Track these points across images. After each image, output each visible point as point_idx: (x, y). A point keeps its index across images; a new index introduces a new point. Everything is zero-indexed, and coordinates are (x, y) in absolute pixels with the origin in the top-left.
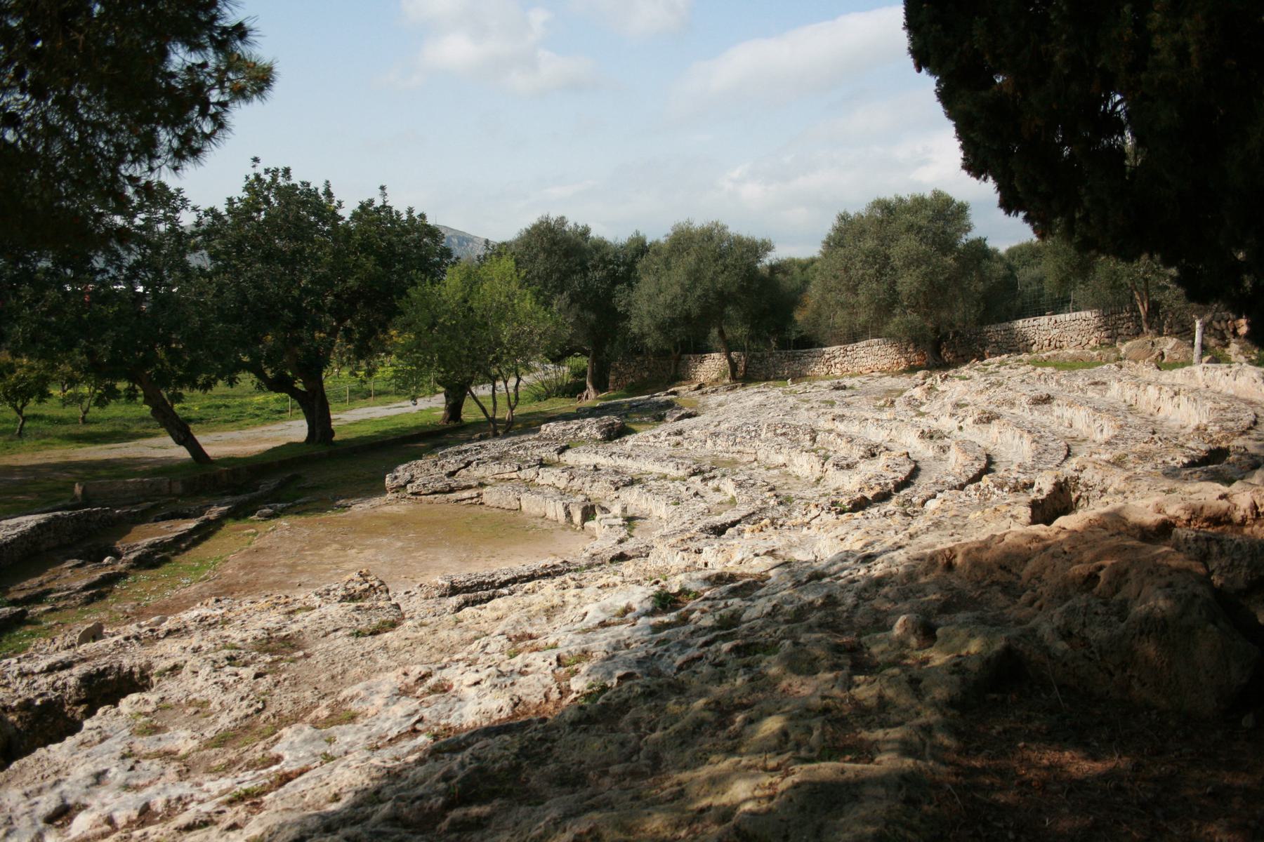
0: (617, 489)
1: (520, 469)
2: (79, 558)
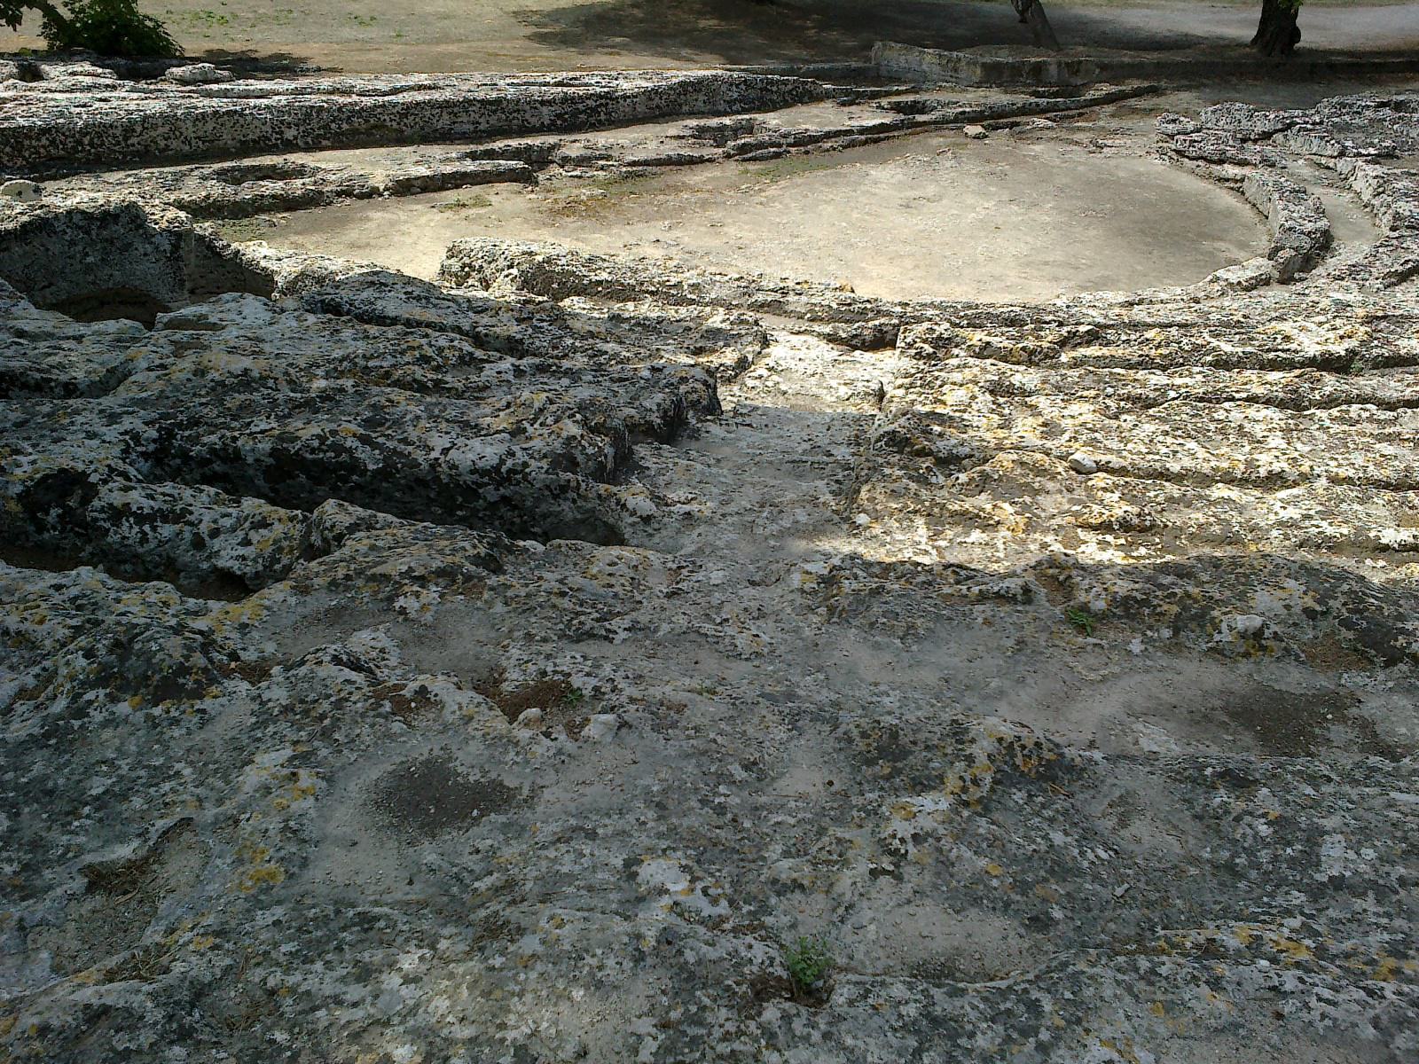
1: (1342, 154)
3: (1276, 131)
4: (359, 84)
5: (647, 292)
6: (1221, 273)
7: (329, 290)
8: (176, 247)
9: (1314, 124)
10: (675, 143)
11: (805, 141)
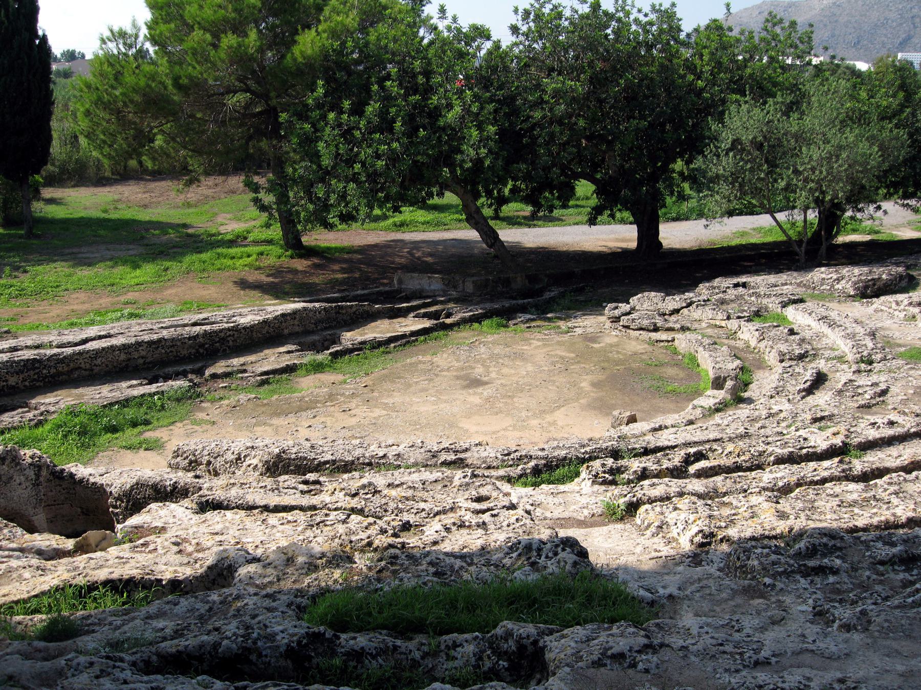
1: (729, 318)
2: (299, 344)
3: (683, 308)
4: (54, 338)
5: (364, 464)
6: (695, 402)
7: (207, 493)
8: (38, 476)
9: (704, 301)
10: (288, 356)
11: (377, 345)
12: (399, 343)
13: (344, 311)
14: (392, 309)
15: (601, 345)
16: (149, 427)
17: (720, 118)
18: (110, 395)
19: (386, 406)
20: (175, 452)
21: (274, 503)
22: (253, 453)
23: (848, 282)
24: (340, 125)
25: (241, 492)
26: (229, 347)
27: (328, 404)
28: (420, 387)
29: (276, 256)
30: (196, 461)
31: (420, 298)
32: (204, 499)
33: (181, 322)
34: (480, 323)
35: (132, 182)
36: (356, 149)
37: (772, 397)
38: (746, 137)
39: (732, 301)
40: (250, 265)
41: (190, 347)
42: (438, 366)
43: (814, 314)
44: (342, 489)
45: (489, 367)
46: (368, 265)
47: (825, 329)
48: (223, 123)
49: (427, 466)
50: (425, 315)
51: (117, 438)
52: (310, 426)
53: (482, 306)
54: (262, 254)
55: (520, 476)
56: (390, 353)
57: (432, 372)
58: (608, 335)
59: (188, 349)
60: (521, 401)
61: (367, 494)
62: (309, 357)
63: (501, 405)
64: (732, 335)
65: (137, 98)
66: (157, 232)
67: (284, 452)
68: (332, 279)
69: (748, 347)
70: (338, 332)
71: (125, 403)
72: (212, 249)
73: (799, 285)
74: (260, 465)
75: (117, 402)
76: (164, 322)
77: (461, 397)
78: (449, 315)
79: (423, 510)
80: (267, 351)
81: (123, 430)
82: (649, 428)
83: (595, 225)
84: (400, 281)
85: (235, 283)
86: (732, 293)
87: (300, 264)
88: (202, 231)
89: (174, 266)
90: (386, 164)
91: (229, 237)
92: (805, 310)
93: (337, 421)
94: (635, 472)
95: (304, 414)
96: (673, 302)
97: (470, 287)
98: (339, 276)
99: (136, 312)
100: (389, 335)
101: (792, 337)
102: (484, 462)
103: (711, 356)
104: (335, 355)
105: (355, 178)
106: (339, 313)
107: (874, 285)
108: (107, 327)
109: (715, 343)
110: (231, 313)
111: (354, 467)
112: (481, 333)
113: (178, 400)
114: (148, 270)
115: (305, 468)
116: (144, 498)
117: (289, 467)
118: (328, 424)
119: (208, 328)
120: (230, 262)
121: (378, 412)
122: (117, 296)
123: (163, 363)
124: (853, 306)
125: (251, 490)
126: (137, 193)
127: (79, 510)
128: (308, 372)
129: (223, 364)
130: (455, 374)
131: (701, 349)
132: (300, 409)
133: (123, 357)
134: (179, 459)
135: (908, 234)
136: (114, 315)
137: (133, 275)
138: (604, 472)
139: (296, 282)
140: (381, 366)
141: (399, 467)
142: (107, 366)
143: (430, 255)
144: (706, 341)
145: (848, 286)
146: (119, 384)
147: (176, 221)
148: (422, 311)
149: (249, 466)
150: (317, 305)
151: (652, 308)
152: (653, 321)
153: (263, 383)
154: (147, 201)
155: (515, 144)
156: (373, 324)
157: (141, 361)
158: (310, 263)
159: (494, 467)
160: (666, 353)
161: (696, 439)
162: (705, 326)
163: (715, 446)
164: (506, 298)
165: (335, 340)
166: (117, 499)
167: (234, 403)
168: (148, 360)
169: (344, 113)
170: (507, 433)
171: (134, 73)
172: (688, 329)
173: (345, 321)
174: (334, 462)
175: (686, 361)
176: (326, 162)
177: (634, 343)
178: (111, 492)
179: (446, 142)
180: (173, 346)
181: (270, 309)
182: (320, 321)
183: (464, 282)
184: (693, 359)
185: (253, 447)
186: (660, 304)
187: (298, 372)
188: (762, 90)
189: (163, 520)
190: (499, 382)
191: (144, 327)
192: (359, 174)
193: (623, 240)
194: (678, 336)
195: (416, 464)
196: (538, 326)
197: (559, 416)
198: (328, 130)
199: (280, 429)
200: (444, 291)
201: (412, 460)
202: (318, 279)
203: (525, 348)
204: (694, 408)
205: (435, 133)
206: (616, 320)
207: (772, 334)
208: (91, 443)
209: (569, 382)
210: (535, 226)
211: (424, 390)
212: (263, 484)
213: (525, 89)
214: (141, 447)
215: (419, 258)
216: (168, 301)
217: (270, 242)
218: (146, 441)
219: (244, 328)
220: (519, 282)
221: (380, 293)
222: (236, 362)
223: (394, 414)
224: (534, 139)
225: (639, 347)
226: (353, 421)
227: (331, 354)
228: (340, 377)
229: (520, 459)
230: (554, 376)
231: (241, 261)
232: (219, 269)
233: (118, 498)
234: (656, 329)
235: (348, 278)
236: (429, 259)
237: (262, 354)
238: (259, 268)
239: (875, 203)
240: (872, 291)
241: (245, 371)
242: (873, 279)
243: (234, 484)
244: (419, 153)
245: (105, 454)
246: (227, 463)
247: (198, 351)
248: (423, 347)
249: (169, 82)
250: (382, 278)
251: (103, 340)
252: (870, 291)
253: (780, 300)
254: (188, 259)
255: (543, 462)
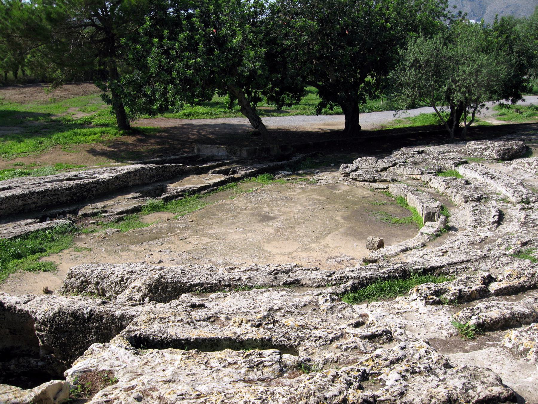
0: (466, 202)
1: (422, 174)
2: (140, 192)
5: (225, 286)
9: (403, 162)
10: (134, 201)
11: (192, 192)
12: (206, 191)
13: (168, 170)
14: (198, 168)
15: (340, 191)
16: (44, 254)
17: (404, 46)
18: (13, 231)
19: (210, 236)
20: (69, 274)
21: (194, 337)
22: (133, 276)
23: (492, 151)
24: (162, 46)
25: (162, 326)
26: (93, 195)
27: (169, 234)
28: (229, 221)
29: (113, 134)
30: (86, 281)
31: (213, 161)
32: (133, 335)
33: (58, 178)
34: (256, 177)
35: (11, 88)
36: (172, 63)
37: (475, 227)
38: (422, 59)
39: (421, 162)
40: (96, 140)
41: (67, 195)
42: (238, 207)
43: (478, 171)
44: (248, 321)
45: (272, 207)
46: (173, 140)
47: (488, 181)
48: (80, 45)
49: (272, 286)
50: (219, 172)
51: (22, 263)
52: (160, 251)
53: (255, 166)
54: (103, 132)
55: (344, 293)
56: (201, 197)
57: (235, 211)
58: (343, 185)
59: (65, 197)
60: (300, 230)
61: (268, 324)
62: (149, 202)
63: (288, 233)
64: (426, 184)
65: (22, 26)
66: (31, 119)
67: (162, 277)
68: (151, 149)
69: (438, 192)
70: (164, 183)
71: (26, 236)
72: (70, 129)
73: (459, 152)
74: (143, 287)
75: (19, 236)
76: (47, 178)
77: (259, 228)
78: (234, 172)
79: (320, 338)
80: (119, 198)
81: (26, 257)
82: (400, 249)
83: (320, 114)
84: (199, 150)
85: (88, 151)
86: (418, 158)
87: (130, 139)
88: (62, 118)
89: (47, 141)
90: (193, 73)
91: (79, 122)
92: (472, 168)
93: (178, 247)
94: (455, 293)
95: (154, 242)
96: (382, 163)
97: (244, 154)
98: (156, 147)
99: (25, 171)
100: (200, 186)
101: (469, 186)
102: (315, 282)
103: (418, 199)
104: (166, 200)
105: (172, 81)
106: (164, 171)
107: (509, 152)
108: (8, 181)
109: (417, 190)
110: (92, 171)
111: (217, 288)
112: (258, 184)
113: (63, 233)
114: (28, 144)
115: (179, 289)
116: (65, 323)
117: (167, 288)
118: (173, 249)
119: (79, 182)
120: (83, 138)
121: (205, 240)
122: (10, 160)
123: (49, 207)
124: (499, 166)
125: (170, 324)
126: (15, 94)
127: (8, 330)
128: (149, 212)
129: (90, 207)
130: (250, 212)
131: (409, 194)
132: (151, 239)
133: (21, 203)
134: (73, 279)
135: (495, 122)
136: (9, 174)
137: (19, 146)
138: (431, 294)
139: (128, 151)
140: (199, 207)
141: (251, 287)
142: (9, 209)
143: (211, 133)
144: (412, 189)
145: (493, 153)
146: (19, 222)
147: (43, 112)
148: (217, 169)
149: (134, 288)
150: (150, 166)
151: (368, 167)
152: (372, 175)
153: (120, 220)
154: (22, 100)
155: (273, 61)
156: (187, 178)
157: (33, 206)
158: (135, 138)
159: (322, 286)
160: (383, 197)
161: (455, 261)
162: (408, 177)
163: (469, 266)
164: (268, 160)
165: (164, 190)
166: (41, 324)
167: (103, 235)
168: (38, 205)
169: (165, 38)
170: (298, 254)
171: (20, 9)
172: (396, 181)
173: (169, 176)
174: (202, 284)
175: (399, 202)
176: (153, 70)
177: (361, 190)
178: (36, 318)
179: (231, 59)
180: (55, 195)
181: (119, 168)
182: (153, 177)
183: (240, 151)
184: (403, 201)
185: (132, 272)
186: (374, 164)
187: (143, 212)
188: (429, 30)
189: (108, 363)
190: (282, 217)
191: (33, 182)
192: (175, 79)
193: (328, 125)
194: (391, 185)
195: (264, 285)
196: (295, 179)
197: (329, 240)
198: (154, 49)
199: (139, 253)
200: (227, 156)
201: (261, 282)
202: (142, 149)
203: (292, 193)
204: (422, 234)
205: (223, 53)
206: (347, 175)
207: (454, 184)
208: (3, 267)
209: (328, 217)
210: (272, 116)
211: (233, 224)
212: (179, 318)
213: (279, 26)
214: (40, 269)
215: (204, 135)
216: (46, 164)
217: (106, 125)
218: (43, 264)
219: (103, 182)
220: (275, 150)
221: (186, 158)
222: (99, 205)
223: (217, 241)
224: (284, 58)
225: (365, 193)
226: (189, 247)
227: (163, 199)
228: (172, 215)
229: (341, 279)
230: (317, 212)
231: (90, 137)
232: (76, 143)
233: (43, 323)
234: (375, 181)
235: (161, 148)
236: (211, 136)
237: (116, 199)
238: (102, 142)
239: (481, 103)
240: (508, 156)
241: (106, 212)
242: (508, 149)
243: (154, 319)
244: (214, 65)
245: (14, 275)
246: (112, 283)
247: (72, 198)
248: (222, 193)
249: (43, 16)
250: (185, 148)
251: (6, 191)
252: (507, 156)
253: (453, 162)
254: (55, 136)
255: (357, 281)
